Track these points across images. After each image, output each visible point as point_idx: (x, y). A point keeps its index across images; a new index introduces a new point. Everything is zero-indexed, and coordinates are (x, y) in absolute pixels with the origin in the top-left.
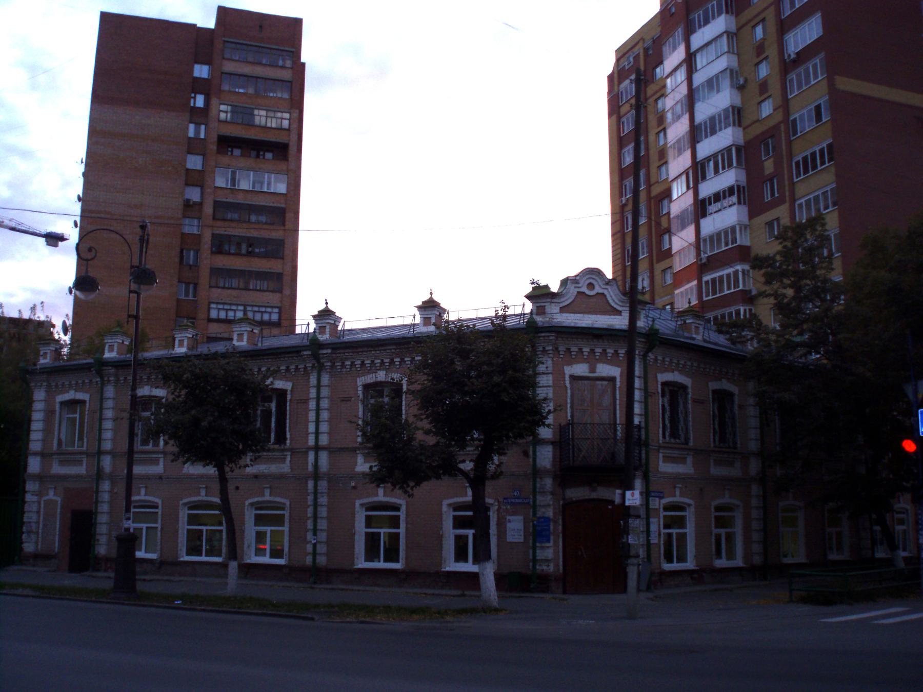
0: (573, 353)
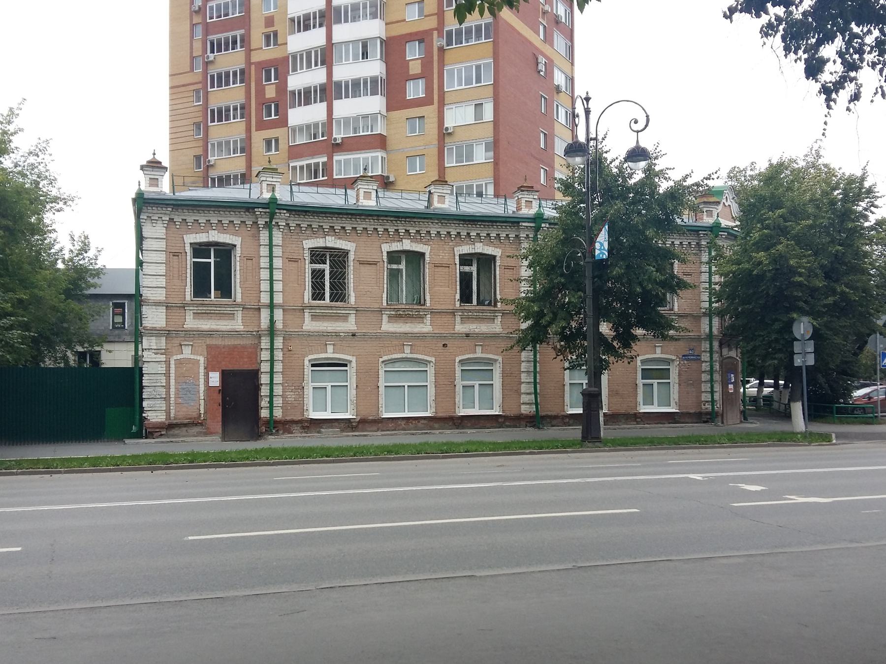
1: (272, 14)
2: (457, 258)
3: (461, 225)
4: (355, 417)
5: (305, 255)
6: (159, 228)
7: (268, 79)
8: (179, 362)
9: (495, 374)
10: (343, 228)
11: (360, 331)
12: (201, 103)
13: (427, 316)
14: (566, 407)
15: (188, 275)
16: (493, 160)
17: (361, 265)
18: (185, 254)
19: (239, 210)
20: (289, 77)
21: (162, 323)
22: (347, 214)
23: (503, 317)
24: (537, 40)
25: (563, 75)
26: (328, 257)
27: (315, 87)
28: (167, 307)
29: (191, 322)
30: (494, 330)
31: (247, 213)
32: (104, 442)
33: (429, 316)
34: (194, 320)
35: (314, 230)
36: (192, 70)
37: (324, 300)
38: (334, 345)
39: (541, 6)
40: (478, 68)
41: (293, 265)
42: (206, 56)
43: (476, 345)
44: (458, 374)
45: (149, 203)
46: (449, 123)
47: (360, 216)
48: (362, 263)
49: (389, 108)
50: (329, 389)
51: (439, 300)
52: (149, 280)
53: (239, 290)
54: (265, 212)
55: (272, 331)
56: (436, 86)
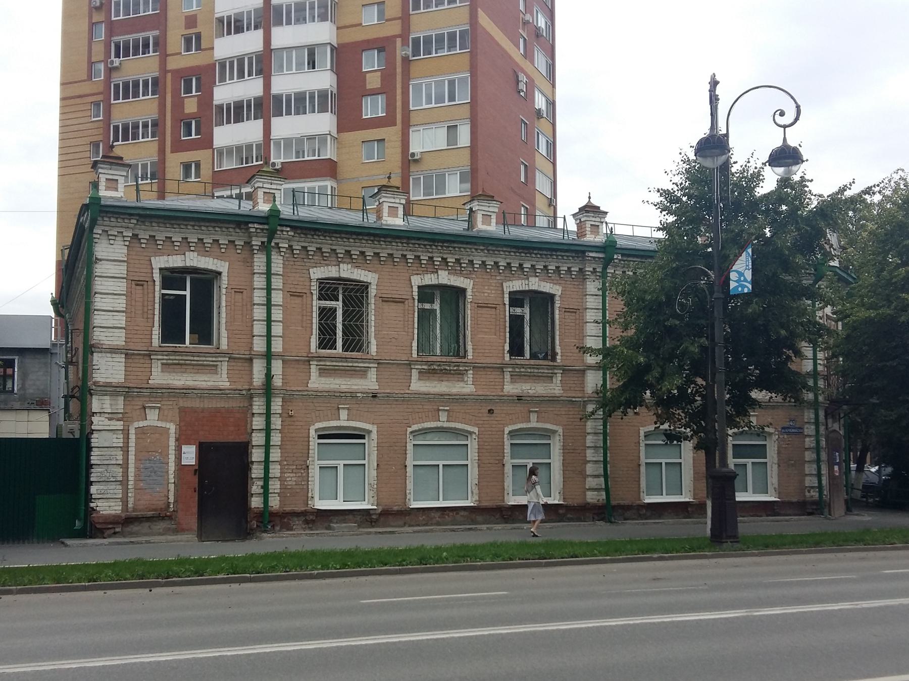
0: (488, 267)
1: (193, 13)
2: (507, 296)
3: (512, 254)
4: (375, 507)
5: (312, 288)
6: (119, 247)
7: (188, 90)
8: (141, 431)
9: (554, 450)
10: (362, 253)
11: (383, 391)
12: (101, 118)
13: (469, 372)
14: (642, 494)
15: (157, 312)
16: (469, 193)
17: (384, 303)
18: (152, 283)
19: (227, 226)
20: (215, 89)
21: (118, 376)
22: (369, 234)
23: (563, 375)
24: (517, 53)
25: (544, 99)
26: (341, 292)
27: (249, 102)
28: (126, 354)
29: (159, 377)
30: (553, 391)
31: (238, 230)
32: (33, 543)
33: (471, 372)
34: (162, 374)
35: (324, 255)
36: (90, 78)
37: (335, 349)
38: (348, 409)
39: (521, 15)
40: (452, 83)
41: (296, 302)
42: (109, 60)
43: (530, 412)
44: (507, 449)
45: (107, 212)
46: (415, 147)
47: (384, 238)
48: (385, 300)
49: (341, 128)
50: (341, 470)
51: (483, 351)
52: (103, 317)
53: (224, 333)
54: (262, 229)
55: (268, 390)
56: (399, 104)
